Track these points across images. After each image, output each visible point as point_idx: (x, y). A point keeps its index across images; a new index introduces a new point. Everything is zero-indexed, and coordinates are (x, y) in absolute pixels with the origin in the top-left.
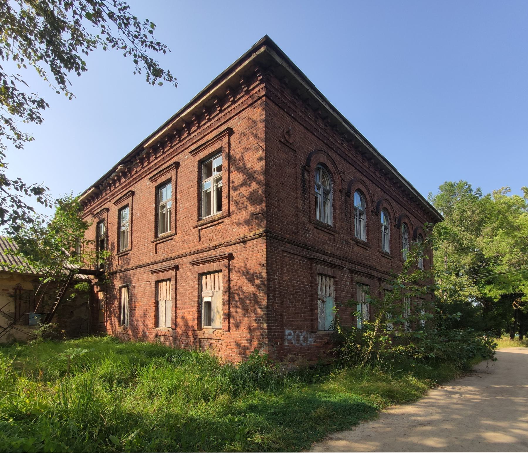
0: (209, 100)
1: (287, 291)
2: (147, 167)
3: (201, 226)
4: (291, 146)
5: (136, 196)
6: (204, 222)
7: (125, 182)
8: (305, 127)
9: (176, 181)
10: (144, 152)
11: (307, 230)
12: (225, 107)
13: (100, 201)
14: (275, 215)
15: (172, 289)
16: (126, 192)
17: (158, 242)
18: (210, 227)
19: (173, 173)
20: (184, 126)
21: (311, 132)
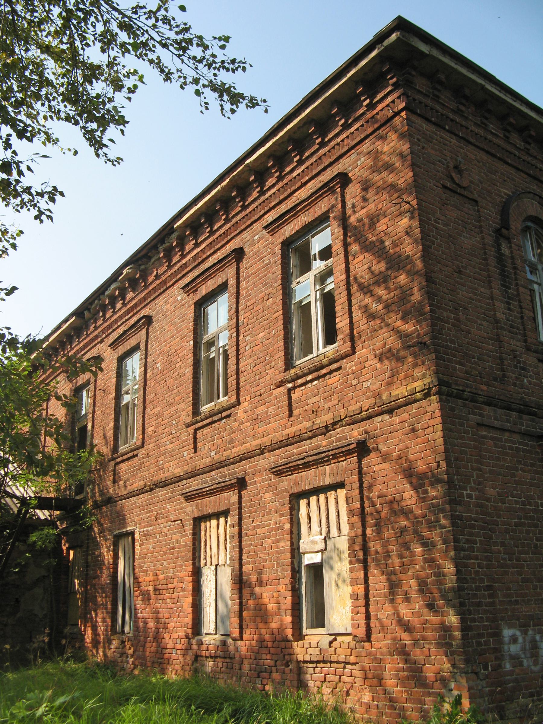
0: (299, 128)
1: (496, 523)
2: (179, 265)
3: (292, 381)
4: (466, 193)
5: (156, 325)
6: (299, 372)
7: (133, 298)
8: (487, 152)
9: (238, 288)
10: (174, 235)
11: (523, 369)
12: (330, 136)
13: (82, 344)
14: (452, 342)
15: (232, 537)
16: (135, 319)
17: (200, 424)
18: (312, 381)
19: (231, 271)
20: (252, 178)
21: (500, 159)
